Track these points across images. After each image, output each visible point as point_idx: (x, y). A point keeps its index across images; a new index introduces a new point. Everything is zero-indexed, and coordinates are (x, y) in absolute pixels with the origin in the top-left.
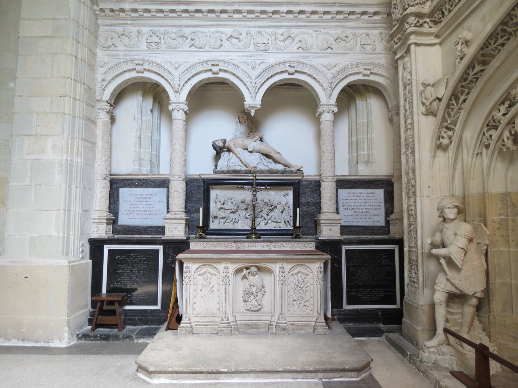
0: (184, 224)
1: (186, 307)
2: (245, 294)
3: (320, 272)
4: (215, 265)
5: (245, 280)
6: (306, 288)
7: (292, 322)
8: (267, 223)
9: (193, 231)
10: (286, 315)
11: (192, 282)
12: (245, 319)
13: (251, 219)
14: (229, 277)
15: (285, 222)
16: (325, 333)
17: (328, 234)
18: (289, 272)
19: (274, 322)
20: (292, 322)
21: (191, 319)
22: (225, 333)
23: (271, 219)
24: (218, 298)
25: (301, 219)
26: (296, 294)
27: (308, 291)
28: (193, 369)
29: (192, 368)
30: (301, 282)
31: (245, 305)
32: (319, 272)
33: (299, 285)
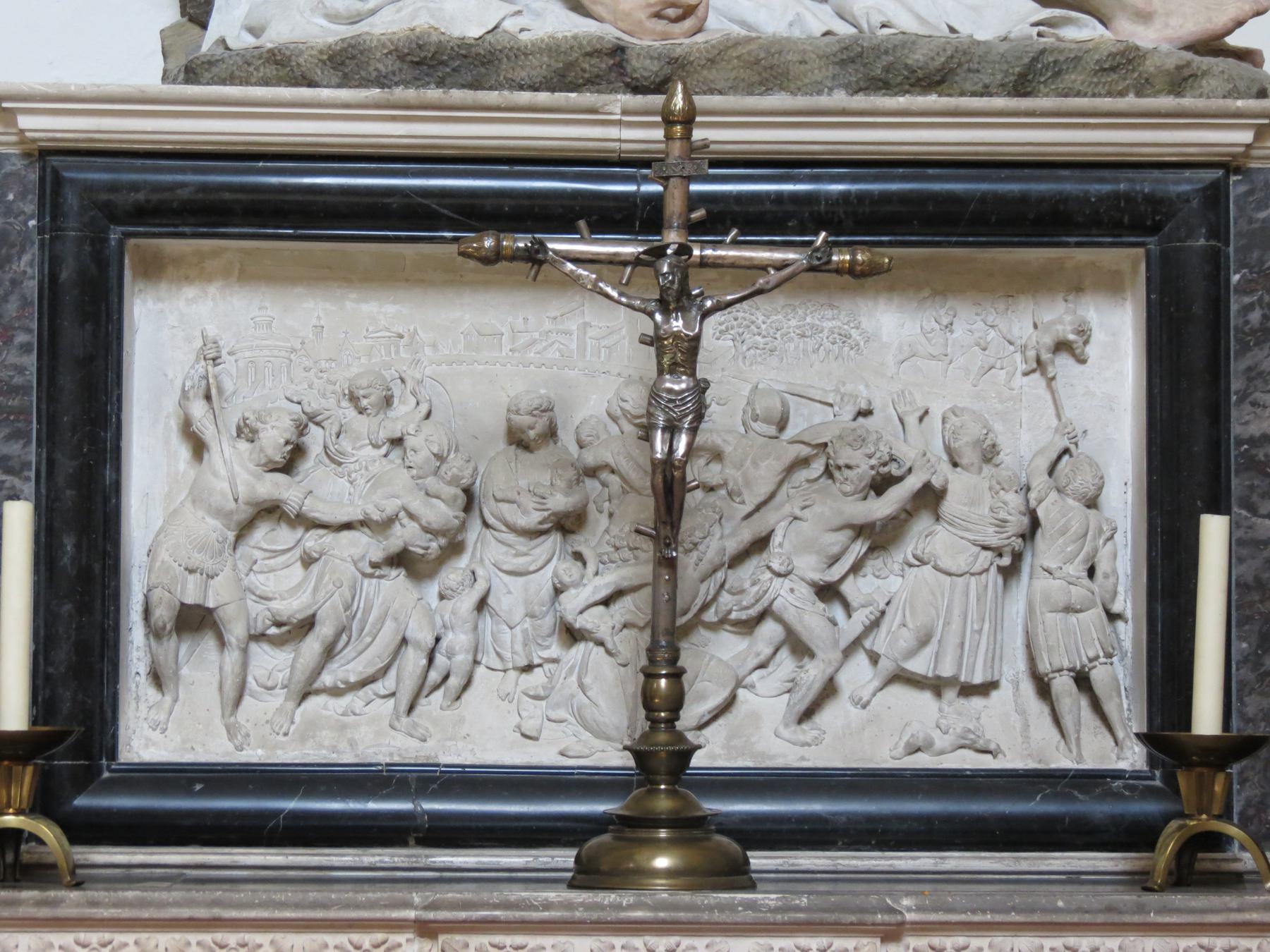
8: (829, 690)
15: (1043, 689)
23: (880, 641)
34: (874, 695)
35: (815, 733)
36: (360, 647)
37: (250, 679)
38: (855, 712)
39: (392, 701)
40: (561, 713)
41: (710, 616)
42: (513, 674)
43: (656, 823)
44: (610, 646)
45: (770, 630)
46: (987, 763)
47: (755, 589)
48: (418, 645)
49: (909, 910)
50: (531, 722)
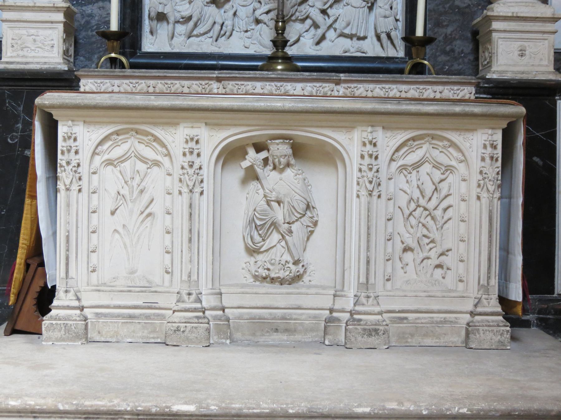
0: (61, 27)
1: (67, 259)
2: (251, 228)
3: (492, 158)
4: (159, 132)
5: (253, 185)
6: (445, 210)
7: (399, 312)
8: (323, 38)
9: (90, 59)
10: (379, 290)
11: (84, 183)
12: (253, 304)
13: (272, 24)
14: (200, 168)
15: (379, 38)
16: (500, 347)
17: (514, 65)
18: (392, 160)
19: (343, 311)
20: (399, 312)
21: (83, 296)
22: (188, 340)
23: (336, 25)
24: (168, 236)
25: (429, 26)
26: (412, 231)
27: (450, 222)
28: (87, 403)
29: (82, 401)
30: (428, 193)
31: (252, 263)
32: (488, 160)
33: (422, 202)
34: (335, 39)
35: (320, 48)
36: (204, 24)
37: (175, 33)
38: (330, 43)
39: (211, 39)
40: (255, 42)
41: (293, 18)
42: (243, 33)
43: (278, 58)
44: (267, 24)
45: (309, 22)
46: (364, 55)
47: (305, 11)
48: (218, 23)
49: (342, 77)
50: (247, 44)
